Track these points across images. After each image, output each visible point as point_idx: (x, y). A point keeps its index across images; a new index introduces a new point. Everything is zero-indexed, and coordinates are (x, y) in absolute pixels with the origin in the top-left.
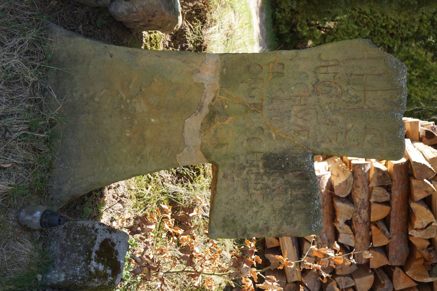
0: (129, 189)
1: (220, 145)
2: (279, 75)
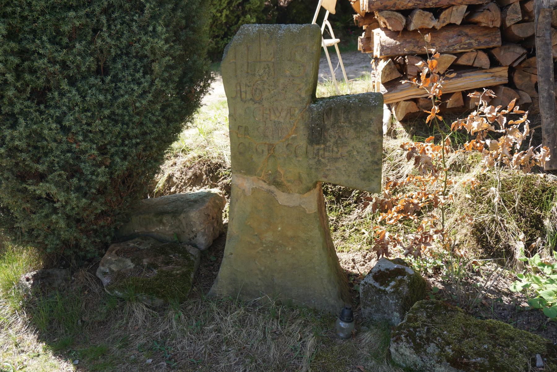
0: (359, 251)
1: (300, 179)
2: (246, 129)
